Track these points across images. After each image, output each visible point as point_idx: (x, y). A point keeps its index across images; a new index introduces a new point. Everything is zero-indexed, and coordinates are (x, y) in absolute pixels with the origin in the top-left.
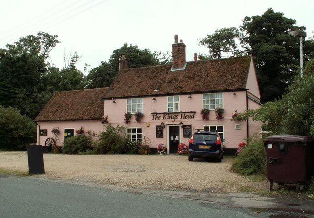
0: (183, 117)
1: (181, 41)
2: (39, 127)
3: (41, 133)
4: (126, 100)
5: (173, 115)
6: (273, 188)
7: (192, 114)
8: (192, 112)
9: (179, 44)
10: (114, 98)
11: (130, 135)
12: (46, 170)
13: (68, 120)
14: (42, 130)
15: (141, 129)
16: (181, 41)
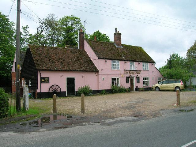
2: (41, 75)
4: (111, 61)
5: (133, 72)
6: (76, 89)
7: (140, 72)
8: (139, 71)
10: (106, 59)
11: (113, 82)
12: (53, 116)
14: (44, 78)
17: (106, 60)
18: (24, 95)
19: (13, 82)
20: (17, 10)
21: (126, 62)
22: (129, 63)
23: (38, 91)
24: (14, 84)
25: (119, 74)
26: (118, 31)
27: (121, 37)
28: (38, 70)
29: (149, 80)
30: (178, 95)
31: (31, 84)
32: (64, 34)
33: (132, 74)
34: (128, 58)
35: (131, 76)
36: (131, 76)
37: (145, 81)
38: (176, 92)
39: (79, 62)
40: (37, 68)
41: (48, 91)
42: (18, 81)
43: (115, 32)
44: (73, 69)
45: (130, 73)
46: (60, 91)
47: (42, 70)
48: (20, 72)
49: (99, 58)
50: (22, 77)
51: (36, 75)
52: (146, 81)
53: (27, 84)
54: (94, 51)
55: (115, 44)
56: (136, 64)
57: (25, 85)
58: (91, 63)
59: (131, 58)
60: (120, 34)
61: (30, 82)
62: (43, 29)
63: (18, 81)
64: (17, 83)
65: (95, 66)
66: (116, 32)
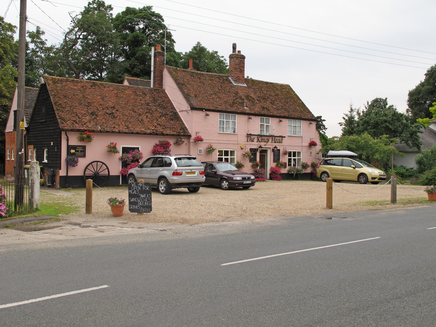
0: (273, 141)
1: (239, 52)
2: (68, 140)
3: (73, 151)
4: (218, 114)
5: (266, 138)
7: (280, 139)
8: (280, 137)
9: (237, 55)
10: (207, 110)
13: (138, 133)
15: (234, 151)
16: (239, 52)
17: (208, 113)
18: (32, 180)
19: (8, 154)
20: (21, 18)
21: (250, 118)
22: (256, 122)
23: (62, 173)
24: (11, 157)
25: (234, 142)
26: (237, 49)
27: (244, 64)
28: (63, 130)
29: (235, 157)
30: (330, 189)
31: (47, 158)
32: (127, 48)
33: (263, 144)
34: (257, 110)
35: (260, 147)
36: (260, 147)
37: (292, 158)
38: (325, 183)
39: (149, 115)
40: (61, 126)
41: (83, 175)
42: (20, 153)
43: (231, 52)
44: (138, 130)
45: (258, 140)
46: (106, 172)
47: (72, 130)
48: (25, 133)
49: (193, 108)
50: (30, 143)
51: (59, 139)
52: (295, 160)
53: (40, 158)
54: (183, 93)
55: (230, 78)
56: (273, 122)
57: (35, 160)
58: (176, 117)
59: (263, 108)
60: (243, 57)
61: (45, 155)
62: (79, 36)
63: (20, 153)
64: (19, 158)
65: (183, 124)
66: (233, 52)
